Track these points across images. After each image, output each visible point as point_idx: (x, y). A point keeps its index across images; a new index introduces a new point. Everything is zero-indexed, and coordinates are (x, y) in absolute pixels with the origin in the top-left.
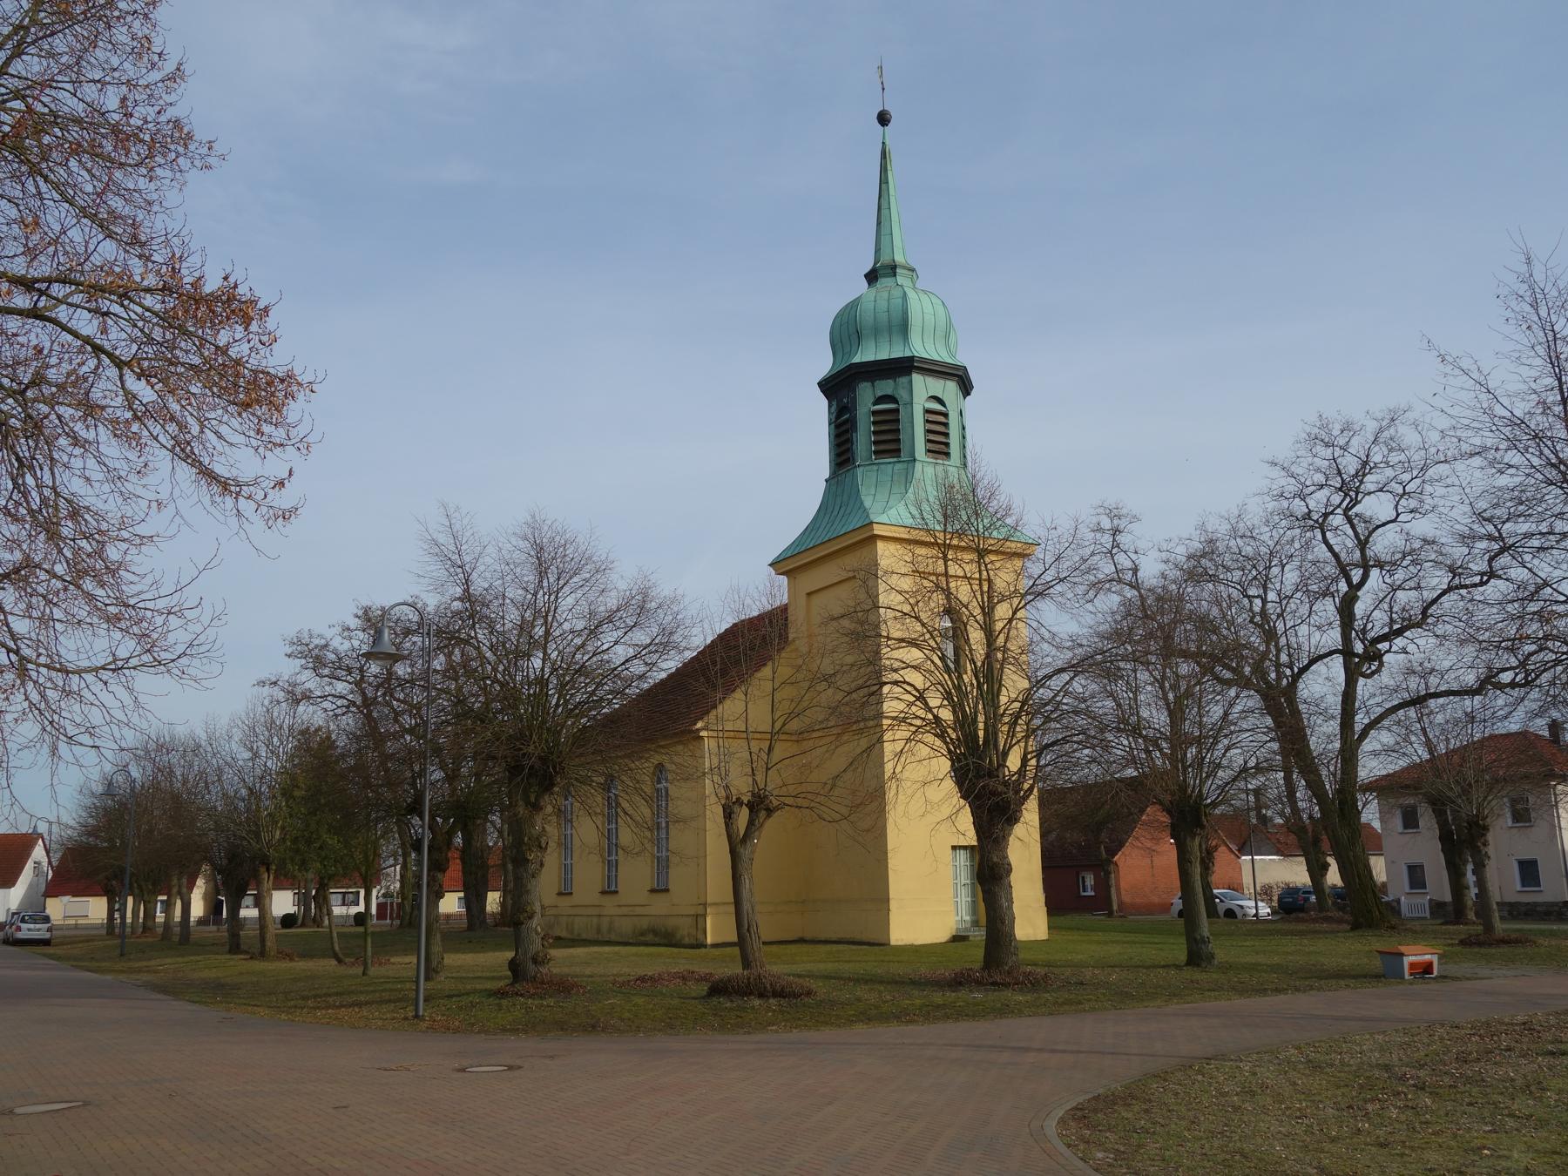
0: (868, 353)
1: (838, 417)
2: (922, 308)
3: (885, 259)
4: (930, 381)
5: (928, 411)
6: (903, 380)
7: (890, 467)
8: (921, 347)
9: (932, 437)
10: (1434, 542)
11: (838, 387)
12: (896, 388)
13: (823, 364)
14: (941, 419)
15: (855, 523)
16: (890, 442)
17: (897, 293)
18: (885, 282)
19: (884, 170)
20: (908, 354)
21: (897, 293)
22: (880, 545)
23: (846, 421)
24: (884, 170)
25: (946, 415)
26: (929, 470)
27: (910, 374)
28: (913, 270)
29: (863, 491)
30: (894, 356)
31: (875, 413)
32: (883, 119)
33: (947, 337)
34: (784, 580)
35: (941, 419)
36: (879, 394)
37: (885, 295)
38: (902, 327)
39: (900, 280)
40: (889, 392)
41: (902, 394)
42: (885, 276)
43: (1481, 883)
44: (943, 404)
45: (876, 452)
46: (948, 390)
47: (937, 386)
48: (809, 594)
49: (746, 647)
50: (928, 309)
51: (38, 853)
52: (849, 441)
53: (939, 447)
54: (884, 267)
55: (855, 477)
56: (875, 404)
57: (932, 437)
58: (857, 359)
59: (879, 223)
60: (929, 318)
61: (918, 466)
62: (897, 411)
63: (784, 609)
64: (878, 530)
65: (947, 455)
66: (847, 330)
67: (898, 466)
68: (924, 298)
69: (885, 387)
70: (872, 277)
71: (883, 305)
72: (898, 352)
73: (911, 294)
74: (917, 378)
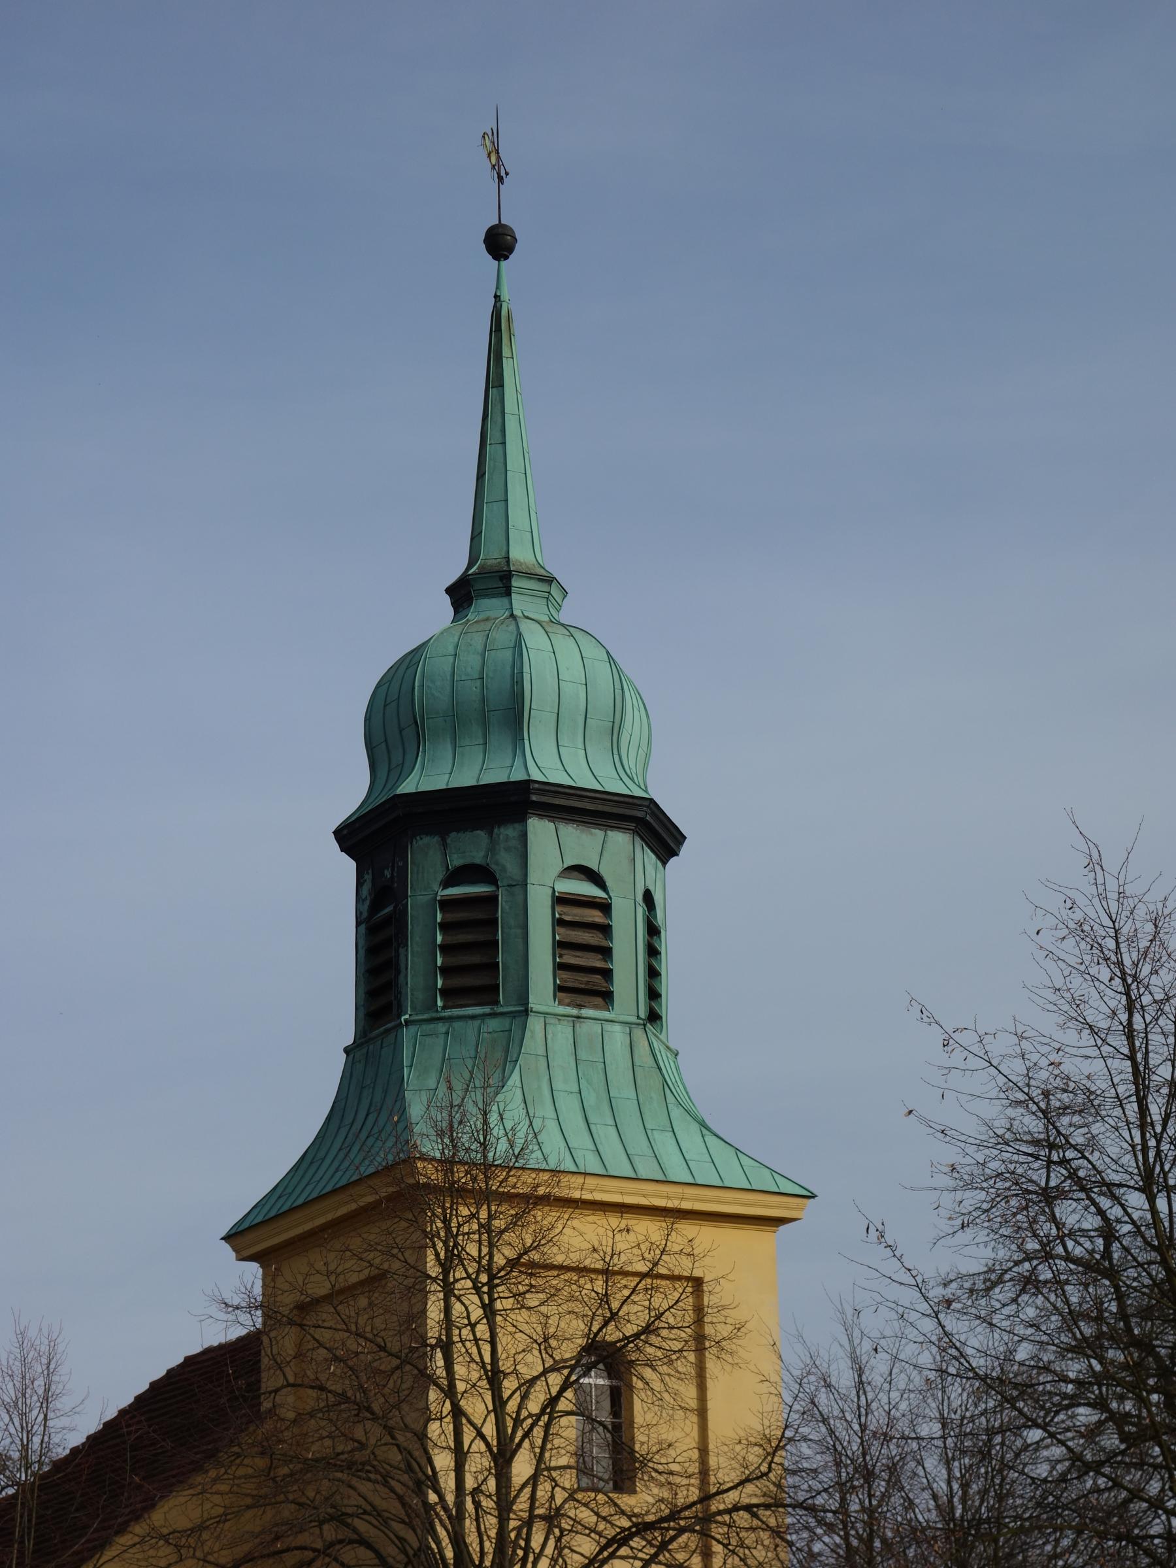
0: (434, 773)
2: (554, 667)
3: (490, 554)
4: (571, 832)
5: (560, 900)
6: (509, 832)
7: (475, 1028)
8: (550, 761)
9: (570, 958)
10: (674, 1515)
11: (372, 838)
12: (492, 849)
13: (349, 789)
14: (596, 916)
15: (384, 1155)
16: (478, 971)
17: (503, 636)
18: (487, 607)
19: (495, 357)
20: (518, 775)
21: (503, 636)
23: (387, 921)
24: (495, 357)
25: (605, 907)
26: (561, 1034)
27: (523, 820)
28: (549, 580)
29: (411, 1077)
30: (489, 778)
32: (499, 243)
33: (615, 730)
34: (253, 1271)
35: (596, 916)
36: (456, 861)
37: (478, 641)
38: (507, 714)
39: (520, 603)
40: (478, 858)
41: (507, 863)
42: (487, 594)
44: (595, 877)
45: (445, 992)
46: (616, 852)
49: (194, 1408)
50: (572, 669)
52: (322, 1297)
53: (586, 982)
54: (484, 573)
55: (397, 1047)
56: (447, 883)
57: (570, 958)
58: (408, 786)
59: (481, 476)
60: (574, 693)
61: (535, 1025)
62: (492, 900)
65: (607, 997)
66: (398, 718)
67: (493, 1024)
68: (564, 644)
69: (470, 847)
70: (461, 594)
71: (471, 662)
72: (497, 773)
73: (534, 638)
74: (540, 830)
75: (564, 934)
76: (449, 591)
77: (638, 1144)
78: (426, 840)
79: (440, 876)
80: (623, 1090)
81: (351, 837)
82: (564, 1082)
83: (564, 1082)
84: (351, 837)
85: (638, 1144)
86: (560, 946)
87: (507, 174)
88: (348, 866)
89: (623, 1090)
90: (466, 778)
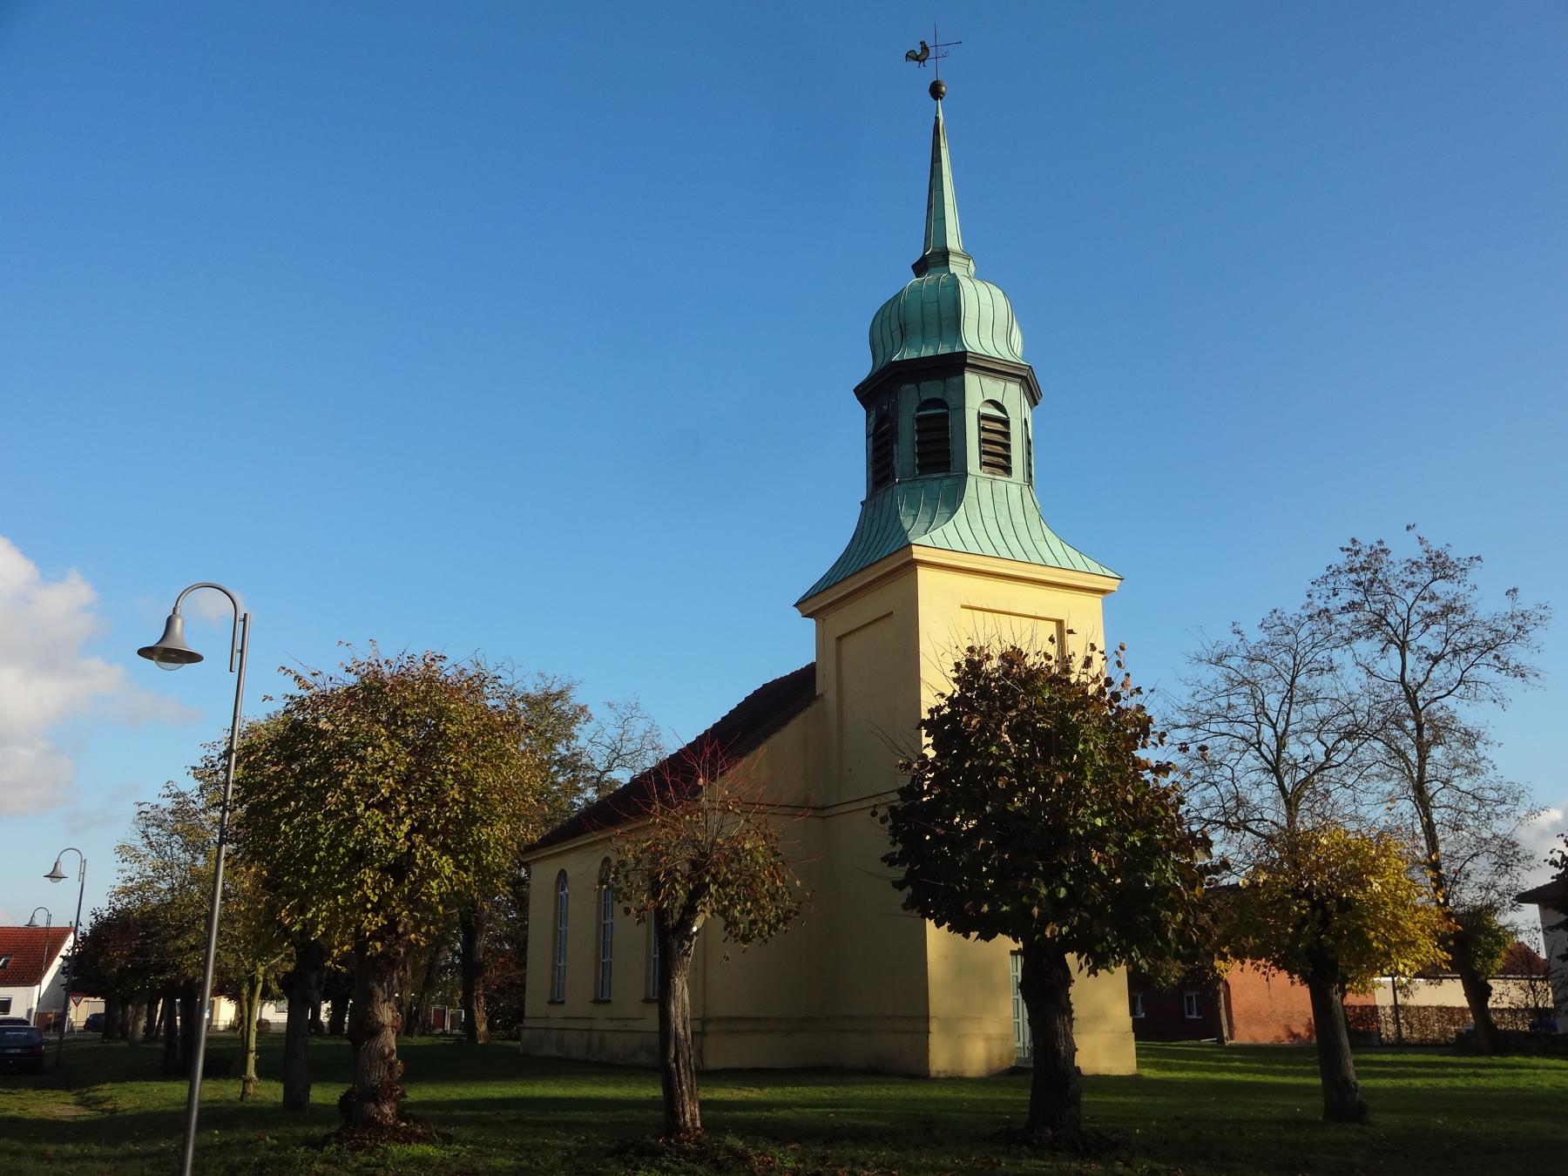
1: (877, 427)
5: (982, 417)
6: (956, 380)
9: (988, 447)
13: (862, 367)
15: (893, 546)
20: (958, 349)
22: (922, 572)
25: (1006, 423)
31: (919, 420)
34: (812, 622)
36: (925, 397)
40: (938, 395)
42: (936, 265)
43: (211, 1019)
47: (996, 388)
48: (839, 639)
51: (69, 942)
52: (890, 454)
53: (999, 462)
56: (919, 410)
57: (988, 447)
59: (930, 208)
61: (971, 481)
62: (945, 416)
63: (810, 670)
64: (918, 554)
65: (1007, 470)
66: (893, 322)
67: (947, 482)
69: (931, 390)
70: (920, 268)
75: (984, 435)
76: (914, 267)
77: (1029, 547)
78: (908, 386)
79: (917, 404)
80: (1018, 518)
81: (865, 393)
82: (988, 513)
83: (988, 513)
84: (865, 393)
85: (1029, 547)
86: (982, 441)
87: (1380, 542)
88: (861, 412)
89: (1018, 518)
90: (928, 352)
